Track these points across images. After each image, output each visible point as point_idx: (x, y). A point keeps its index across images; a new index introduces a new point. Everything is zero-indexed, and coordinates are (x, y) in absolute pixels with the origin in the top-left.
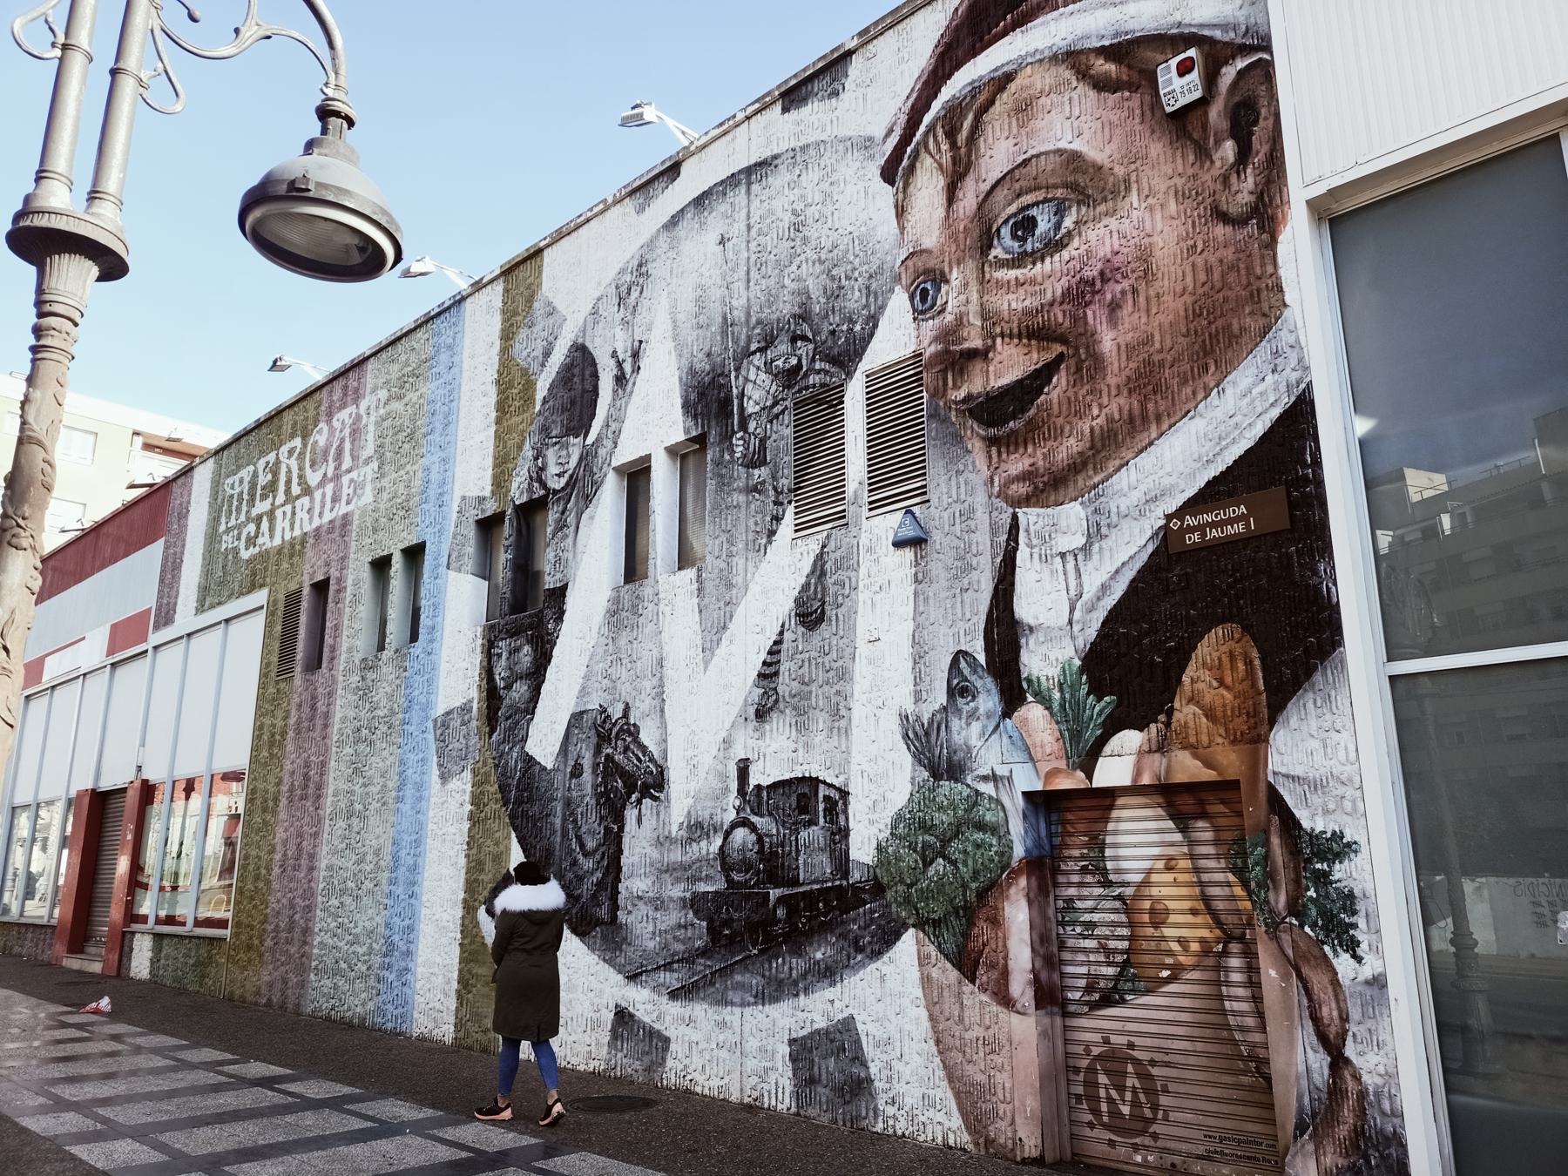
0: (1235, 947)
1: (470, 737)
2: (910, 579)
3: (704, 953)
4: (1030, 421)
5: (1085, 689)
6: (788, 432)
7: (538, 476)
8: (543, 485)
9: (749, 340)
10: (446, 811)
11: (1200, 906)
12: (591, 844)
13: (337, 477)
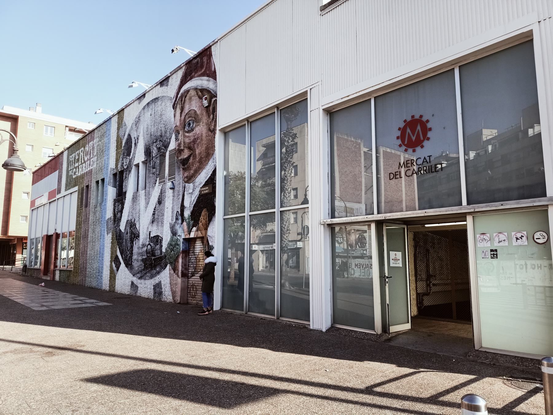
1: (111, 224)
3: (144, 270)
6: (158, 161)
7: (122, 166)
10: (108, 239)
13: (90, 159)
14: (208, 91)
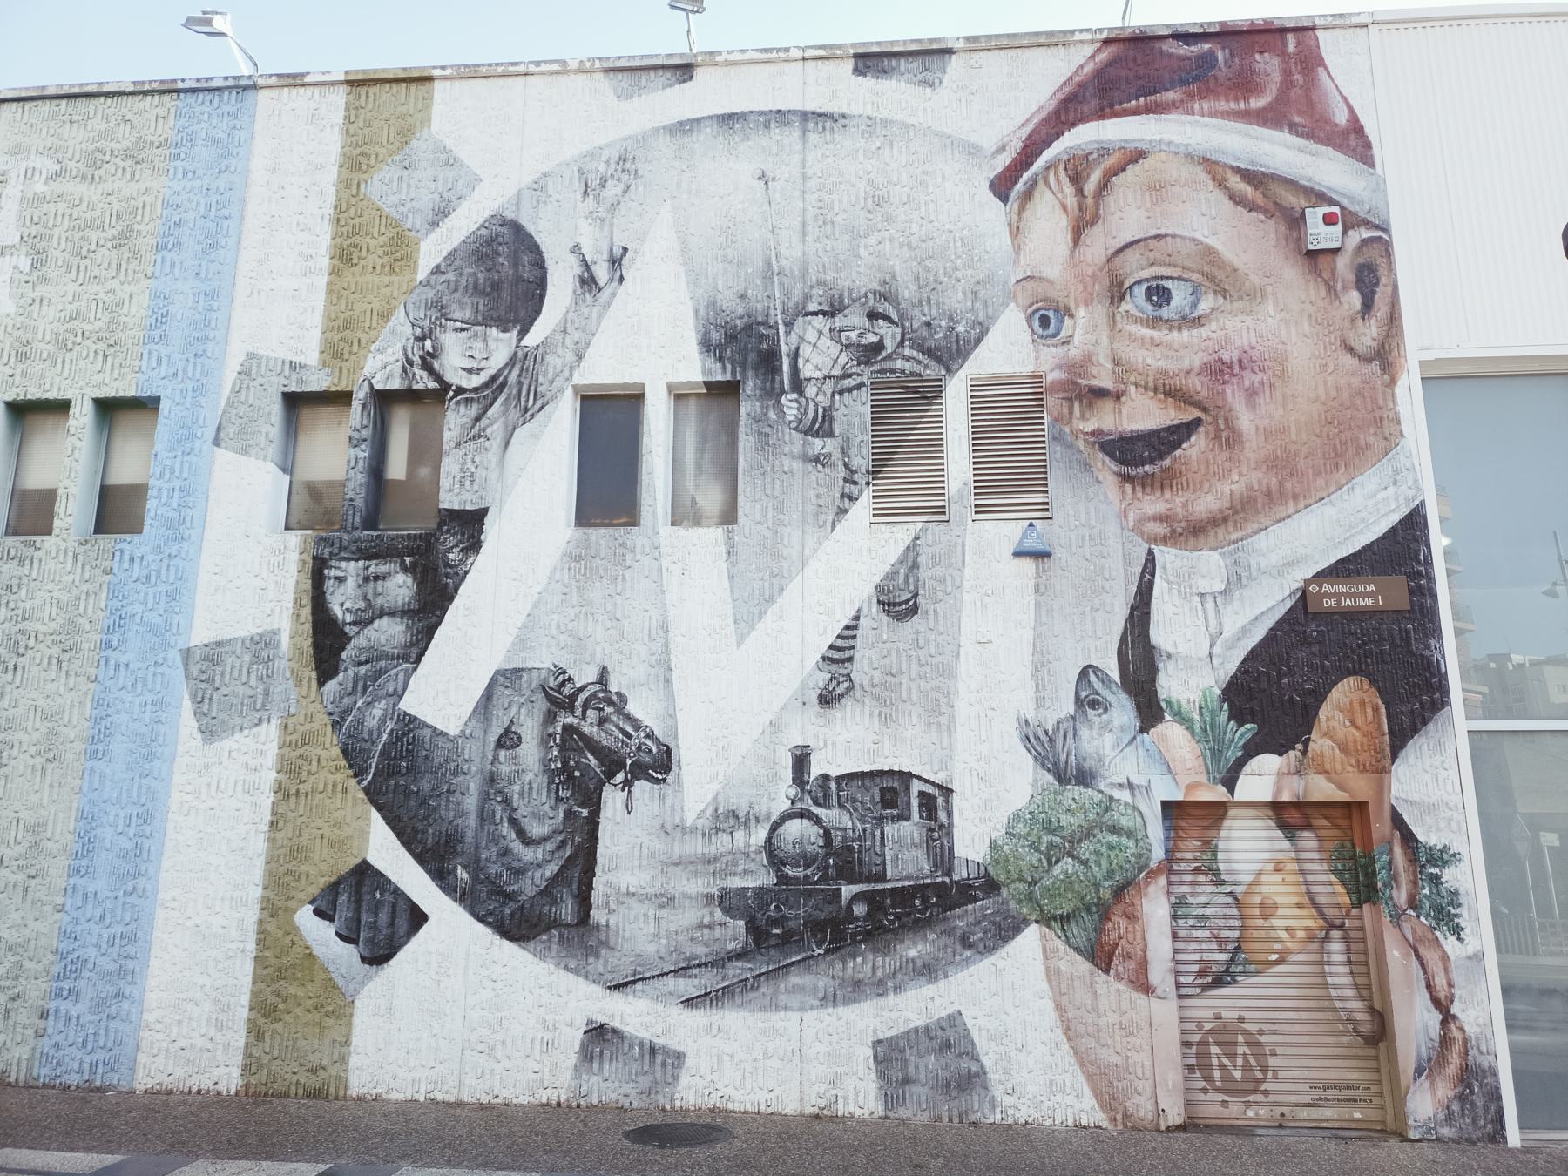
0: (1335, 934)
2: (1031, 590)
3: (739, 955)
4: (1165, 470)
5: (1225, 715)
9: (807, 298)
11: (1306, 901)
12: (536, 830)
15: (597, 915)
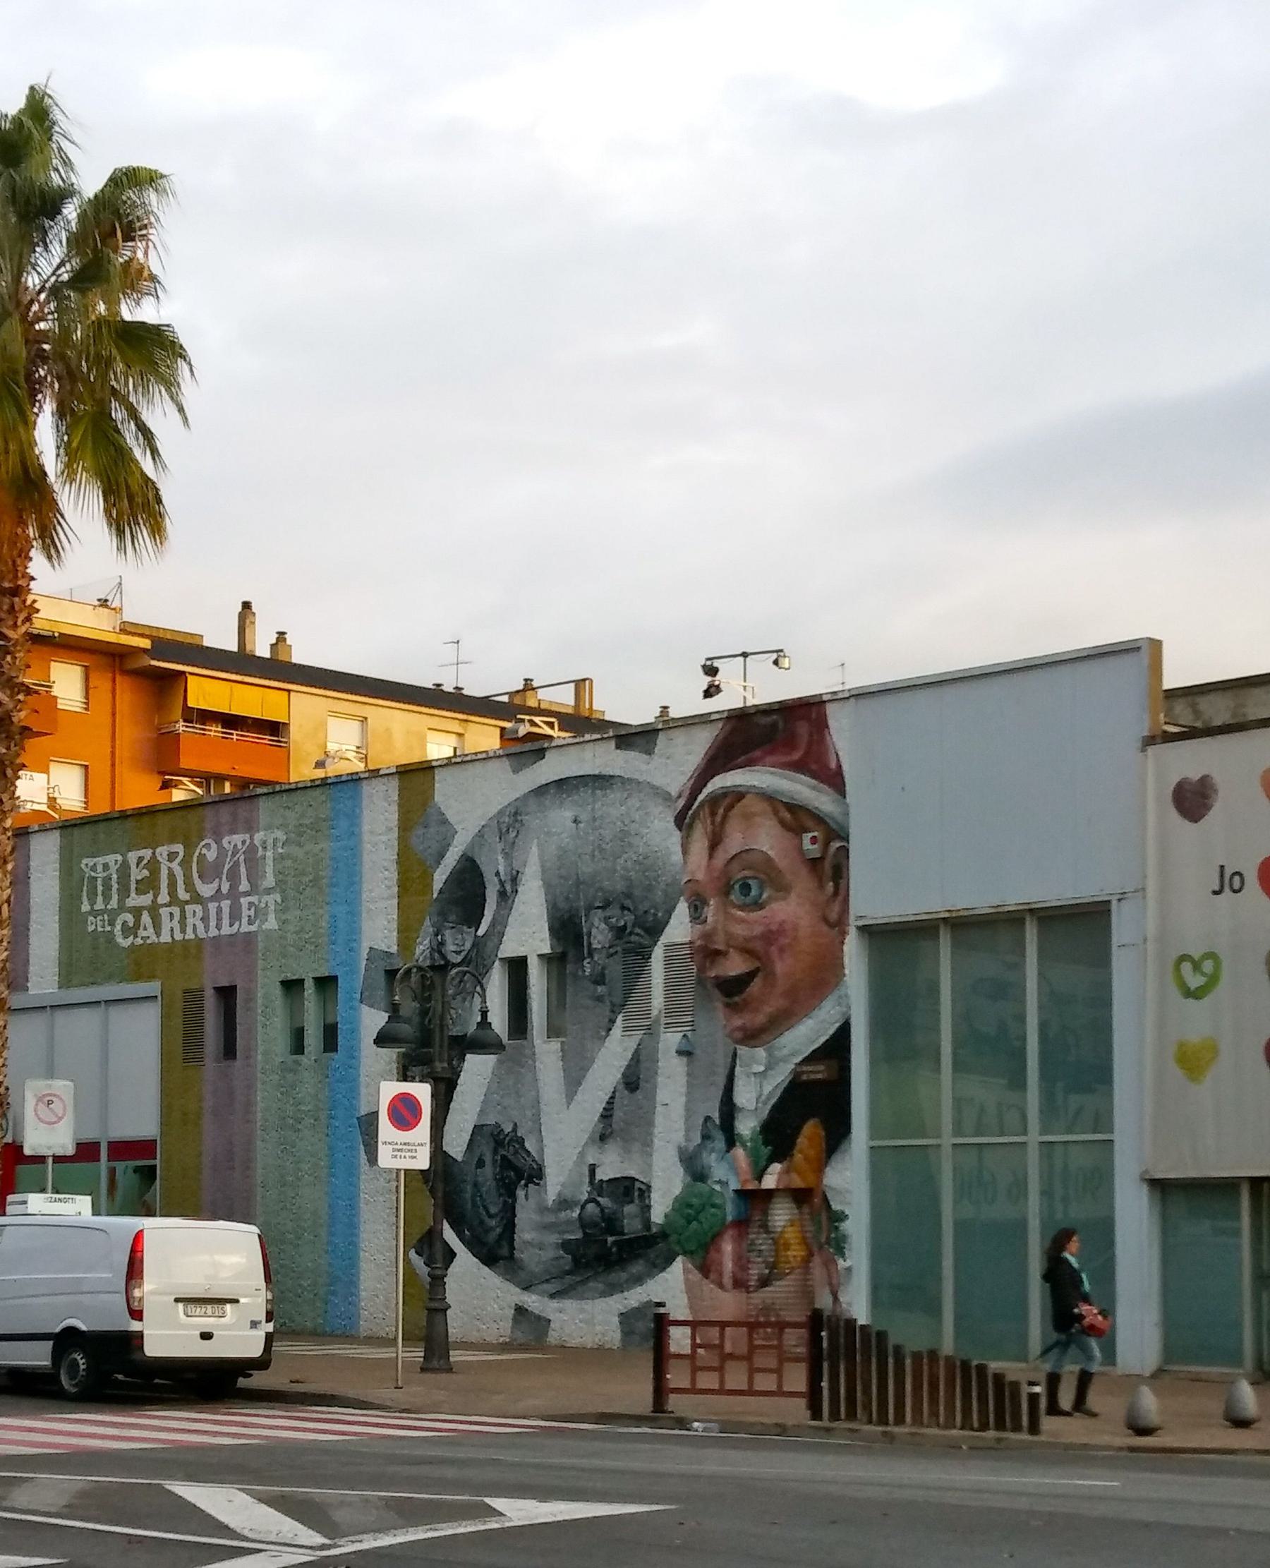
4: (744, 1000)
6: (620, 968)
7: (439, 948)
8: (443, 957)
12: (493, 1210)
14: (819, 819)
15: (517, 1254)
